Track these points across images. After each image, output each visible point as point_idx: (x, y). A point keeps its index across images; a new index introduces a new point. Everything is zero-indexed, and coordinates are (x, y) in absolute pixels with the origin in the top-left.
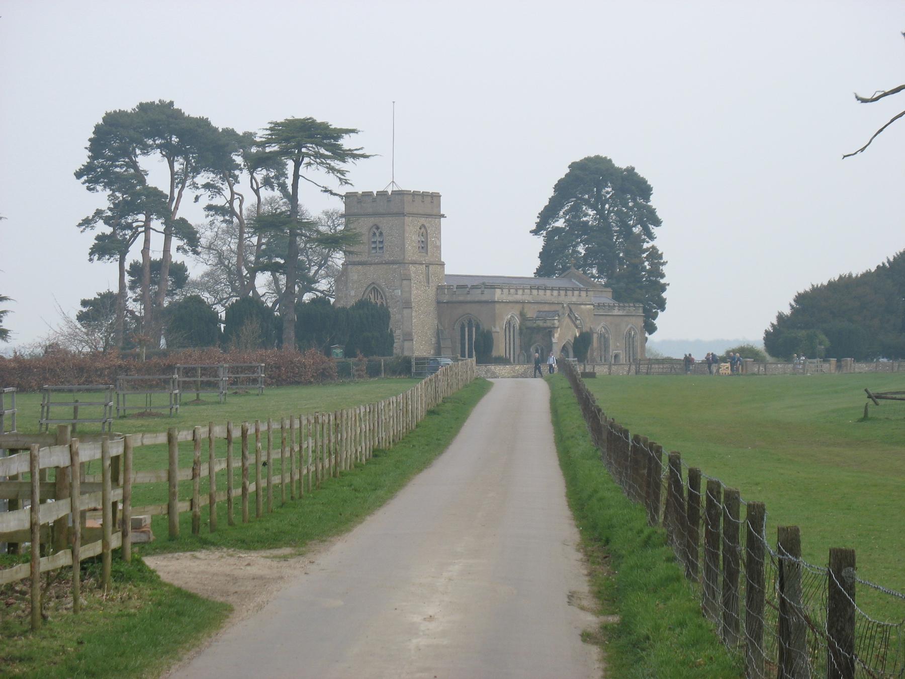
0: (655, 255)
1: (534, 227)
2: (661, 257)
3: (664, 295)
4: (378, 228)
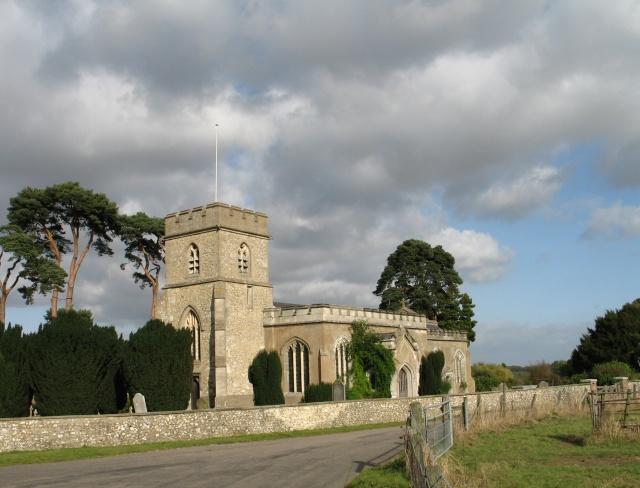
0: (466, 301)
1: (375, 289)
2: (471, 303)
3: (474, 329)
4: (195, 247)
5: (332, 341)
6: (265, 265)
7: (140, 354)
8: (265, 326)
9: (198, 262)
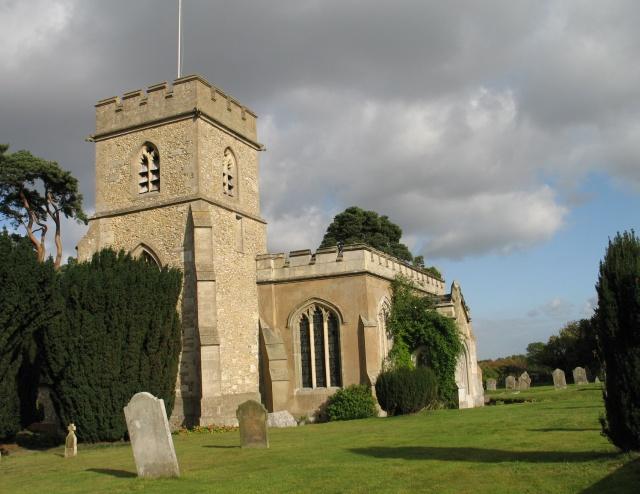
4: (151, 147)
5: (375, 306)
6: (255, 188)
7: (86, 313)
8: (258, 283)
9: (156, 172)
